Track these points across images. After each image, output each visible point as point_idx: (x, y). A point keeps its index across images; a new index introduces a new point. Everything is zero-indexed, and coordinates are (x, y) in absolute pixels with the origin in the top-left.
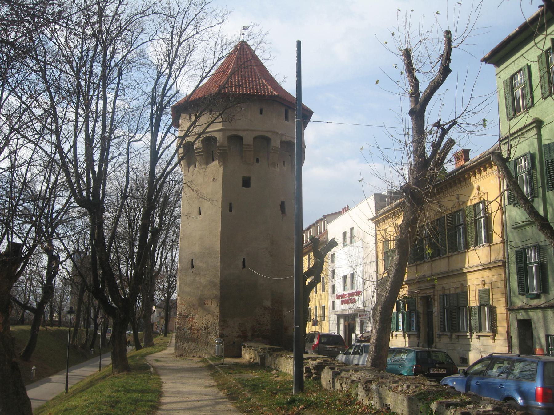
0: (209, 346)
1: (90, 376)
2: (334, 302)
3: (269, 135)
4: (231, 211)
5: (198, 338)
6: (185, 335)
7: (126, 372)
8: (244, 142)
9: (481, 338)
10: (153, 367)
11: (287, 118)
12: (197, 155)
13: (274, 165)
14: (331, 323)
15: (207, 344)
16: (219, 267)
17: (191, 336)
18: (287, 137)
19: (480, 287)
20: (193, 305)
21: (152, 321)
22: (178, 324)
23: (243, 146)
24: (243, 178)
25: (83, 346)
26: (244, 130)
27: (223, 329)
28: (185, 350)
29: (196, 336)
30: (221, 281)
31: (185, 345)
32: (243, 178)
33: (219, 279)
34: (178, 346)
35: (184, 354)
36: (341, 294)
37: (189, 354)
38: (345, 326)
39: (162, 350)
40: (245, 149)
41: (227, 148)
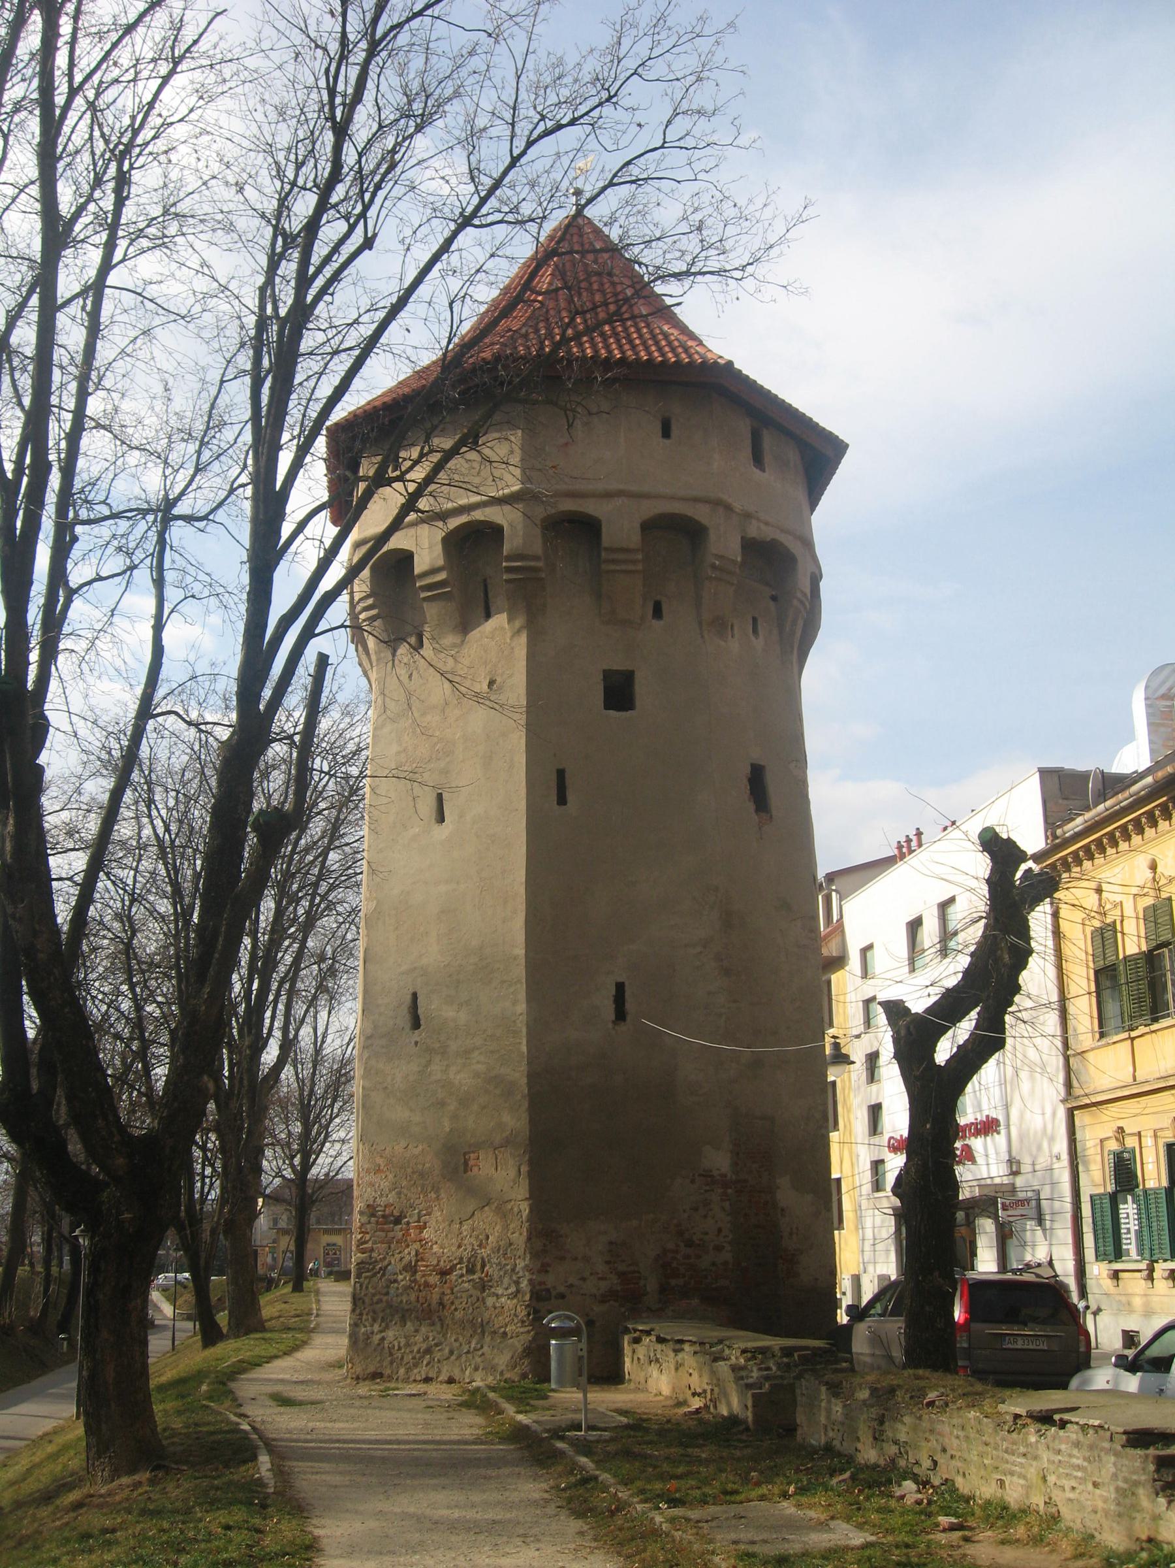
0: (488, 1339)
1: (47, 1437)
3: (701, 514)
4: (562, 800)
5: (441, 1304)
6: (392, 1291)
7: (144, 1476)
8: (606, 541)
9: (1121, 1275)
10: (271, 1447)
11: (758, 459)
13: (721, 626)
14: (869, 1234)
15: (480, 1328)
16: (524, 1018)
17: (413, 1297)
18: (763, 527)
19: (1113, 1146)
20: (422, 1175)
24: (607, 675)
25: (36, 1328)
26: (608, 495)
27: (544, 1269)
28: (391, 1354)
29: (435, 1298)
30: (532, 1077)
31: (390, 1334)
32: (607, 675)
33: (524, 1067)
34: (361, 1338)
35: (387, 1372)
37: (408, 1370)
40: (612, 567)
41: (540, 564)
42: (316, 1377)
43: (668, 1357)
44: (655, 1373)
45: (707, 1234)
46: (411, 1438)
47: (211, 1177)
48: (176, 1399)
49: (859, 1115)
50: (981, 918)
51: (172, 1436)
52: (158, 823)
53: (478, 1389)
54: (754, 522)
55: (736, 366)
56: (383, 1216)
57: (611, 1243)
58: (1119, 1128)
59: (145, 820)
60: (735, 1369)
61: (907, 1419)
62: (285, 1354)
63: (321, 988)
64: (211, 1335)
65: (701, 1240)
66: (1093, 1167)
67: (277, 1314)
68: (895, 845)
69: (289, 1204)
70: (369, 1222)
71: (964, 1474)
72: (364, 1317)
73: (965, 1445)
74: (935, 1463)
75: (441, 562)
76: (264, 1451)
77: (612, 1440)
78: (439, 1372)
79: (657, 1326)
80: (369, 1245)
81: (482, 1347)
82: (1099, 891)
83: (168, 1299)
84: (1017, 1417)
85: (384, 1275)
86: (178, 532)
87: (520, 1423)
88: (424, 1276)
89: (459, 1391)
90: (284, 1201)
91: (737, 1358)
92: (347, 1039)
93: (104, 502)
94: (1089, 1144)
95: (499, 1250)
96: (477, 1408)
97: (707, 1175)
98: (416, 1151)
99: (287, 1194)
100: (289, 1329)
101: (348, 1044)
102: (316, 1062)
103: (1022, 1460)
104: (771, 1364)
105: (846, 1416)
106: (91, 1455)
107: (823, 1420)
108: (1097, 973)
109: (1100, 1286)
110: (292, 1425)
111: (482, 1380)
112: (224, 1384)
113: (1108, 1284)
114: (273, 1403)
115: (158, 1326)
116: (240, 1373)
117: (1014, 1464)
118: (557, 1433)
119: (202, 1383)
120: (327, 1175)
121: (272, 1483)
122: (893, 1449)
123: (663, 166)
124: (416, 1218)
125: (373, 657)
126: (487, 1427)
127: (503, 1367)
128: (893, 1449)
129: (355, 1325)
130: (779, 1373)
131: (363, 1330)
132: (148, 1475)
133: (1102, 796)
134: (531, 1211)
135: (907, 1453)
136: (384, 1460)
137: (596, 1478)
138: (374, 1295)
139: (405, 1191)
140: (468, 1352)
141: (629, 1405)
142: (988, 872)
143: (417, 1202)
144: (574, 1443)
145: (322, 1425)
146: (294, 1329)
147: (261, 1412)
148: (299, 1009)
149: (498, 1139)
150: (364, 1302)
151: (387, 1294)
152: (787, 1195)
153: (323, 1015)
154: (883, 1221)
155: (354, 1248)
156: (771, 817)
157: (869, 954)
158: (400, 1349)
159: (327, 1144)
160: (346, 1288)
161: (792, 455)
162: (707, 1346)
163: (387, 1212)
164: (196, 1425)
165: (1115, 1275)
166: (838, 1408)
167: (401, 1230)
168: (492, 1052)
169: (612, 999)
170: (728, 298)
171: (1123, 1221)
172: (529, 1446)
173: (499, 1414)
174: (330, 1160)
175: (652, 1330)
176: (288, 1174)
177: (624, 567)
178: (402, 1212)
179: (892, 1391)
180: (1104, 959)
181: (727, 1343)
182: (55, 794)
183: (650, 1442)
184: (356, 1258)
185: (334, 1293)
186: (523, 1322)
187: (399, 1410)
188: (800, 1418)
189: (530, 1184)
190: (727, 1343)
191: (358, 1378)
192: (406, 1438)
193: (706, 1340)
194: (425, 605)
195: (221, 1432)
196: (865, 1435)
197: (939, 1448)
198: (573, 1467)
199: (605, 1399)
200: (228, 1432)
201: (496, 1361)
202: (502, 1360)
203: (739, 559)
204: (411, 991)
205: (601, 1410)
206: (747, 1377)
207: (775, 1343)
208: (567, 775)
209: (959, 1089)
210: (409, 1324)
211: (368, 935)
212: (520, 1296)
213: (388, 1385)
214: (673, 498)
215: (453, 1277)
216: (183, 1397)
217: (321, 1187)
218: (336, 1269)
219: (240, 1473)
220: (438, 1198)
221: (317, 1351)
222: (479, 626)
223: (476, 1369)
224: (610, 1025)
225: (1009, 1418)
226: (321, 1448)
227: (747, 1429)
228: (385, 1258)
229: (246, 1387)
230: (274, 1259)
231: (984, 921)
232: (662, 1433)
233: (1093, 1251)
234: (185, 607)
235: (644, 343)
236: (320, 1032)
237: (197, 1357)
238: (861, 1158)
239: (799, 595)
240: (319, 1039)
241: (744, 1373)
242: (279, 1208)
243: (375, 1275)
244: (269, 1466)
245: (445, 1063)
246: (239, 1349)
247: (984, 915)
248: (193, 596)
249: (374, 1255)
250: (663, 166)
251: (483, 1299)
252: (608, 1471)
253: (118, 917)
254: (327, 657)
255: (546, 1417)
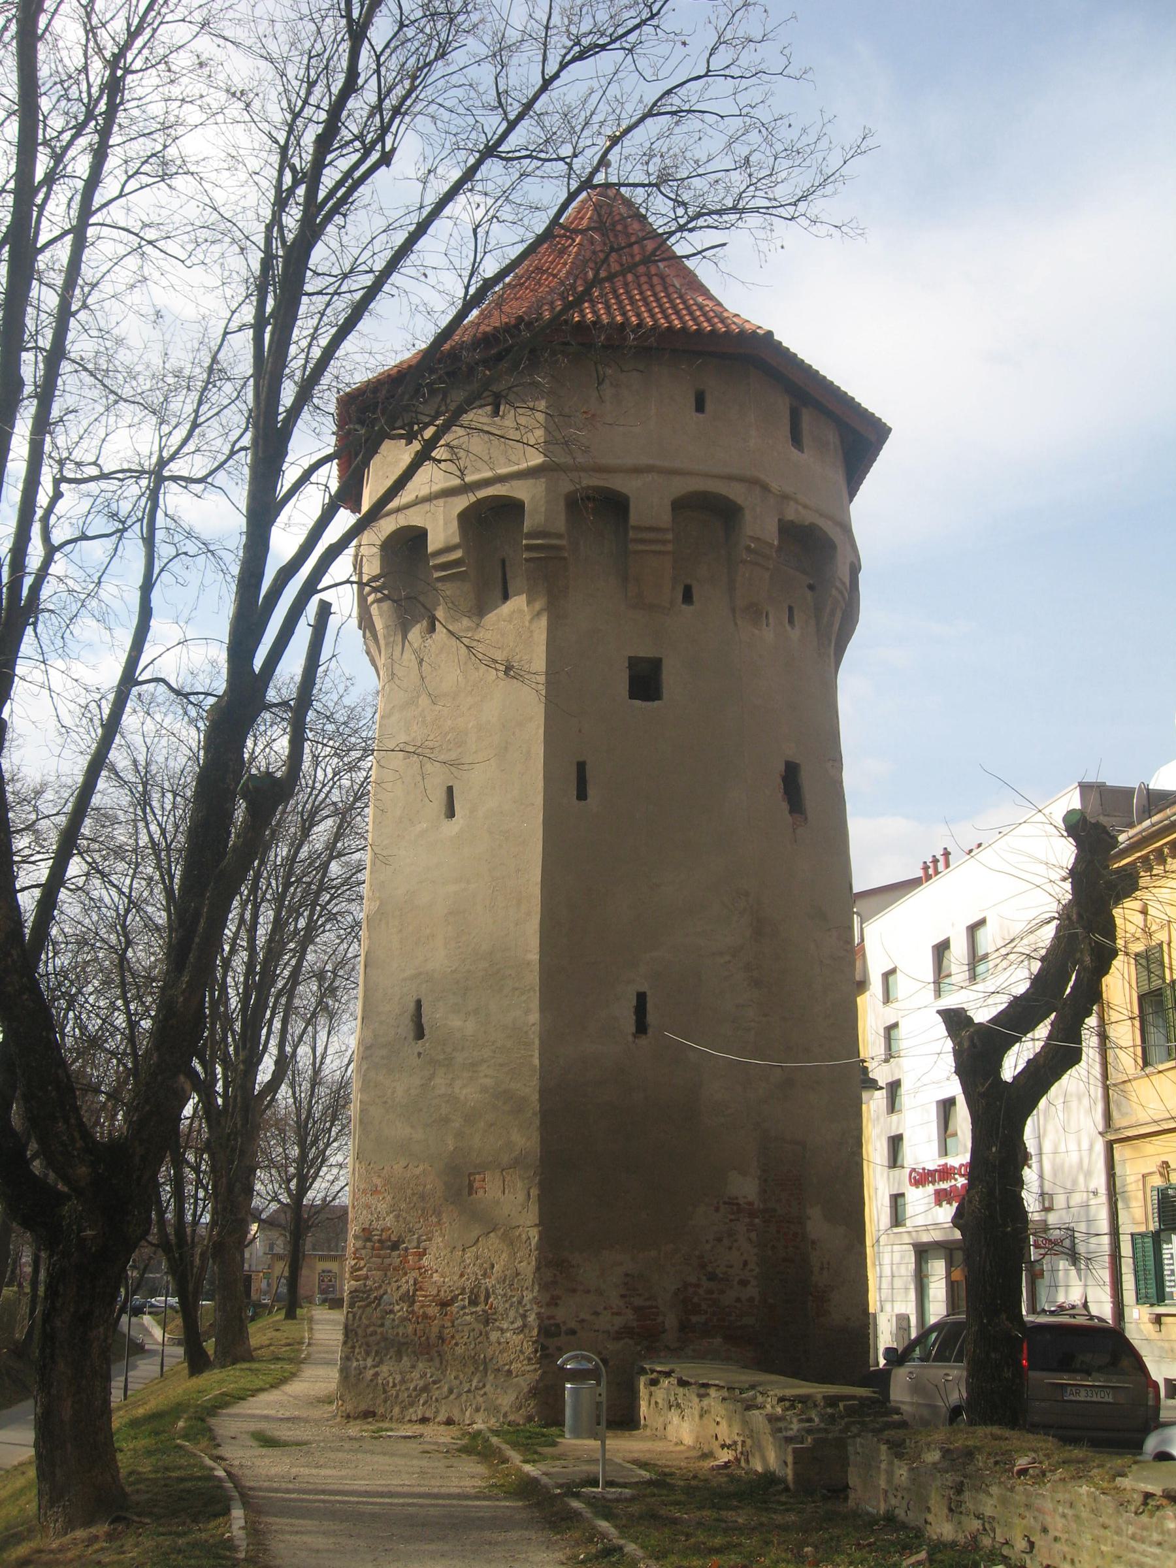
0: (491, 1377)
2: (897, 1200)
3: (735, 492)
4: (582, 795)
5: (441, 1338)
6: (388, 1323)
7: (102, 1529)
8: (633, 519)
9: (1164, 1319)
11: (796, 439)
12: (439, 579)
13: (755, 613)
15: (481, 1365)
16: (537, 1028)
17: (410, 1329)
18: (800, 508)
19: (1157, 1181)
20: (422, 1197)
21: (246, 1267)
22: (357, 1279)
23: (631, 534)
24: (633, 662)
26: (637, 470)
27: (554, 1302)
28: (385, 1392)
29: (435, 1330)
30: (544, 1093)
31: (384, 1369)
32: (633, 662)
33: (535, 1082)
35: (380, 1410)
36: (931, 1166)
38: (952, 1286)
39: (284, 1381)
40: (641, 547)
42: (303, 1413)
43: (693, 1404)
44: (676, 1420)
45: (731, 1267)
46: (406, 1489)
47: (204, 1200)
48: (150, 1435)
49: (878, 1145)
50: (1054, 918)
51: (138, 1482)
52: (154, 828)
53: (479, 1432)
54: (792, 503)
55: (776, 337)
56: (380, 1241)
57: (627, 1275)
58: (1164, 1162)
59: (141, 825)
60: (771, 1419)
61: (994, 1490)
62: (272, 1387)
63: (321, 1005)
64: (197, 1362)
65: (725, 1273)
66: (1133, 1204)
67: (267, 1342)
68: (921, 865)
69: (284, 1228)
70: (364, 1247)
71: (1072, 1561)
72: (357, 1350)
73: (1074, 1526)
74: (1032, 1544)
75: (456, 540)
76: (239, 1504)
77: (632, 1499)
78: (437, 1412)
79: (677, 1367)
80: (364, 1272)
81: (484, 1386)
82: (1144, 912)
83: (159, 1323)
84: (1148, 1496)
85: (379, 1305)
86: (174, 498)
87: (527, 1475)
88: (422, 1307)
89: (458, 1434)
90: (279, 1226)
91: (773, 1407)
92: (346, 1061)
93: (95, 463)
94: (1130, 1179)
95: (504, 1281)
96: (479, 1454)
97: (732, 1203)
98: (418, 1171)
99: (282, 1218)
100: (278, 1359)
101: (348, 1065)
102: (315, 1081)
103: (1157, 1550)
104: (813, 1414)
105: (913, 1480)
106: (44, 1502)
107: (883, 1484)
108: (1141, 998)
109: (1140, 1331)
110: (273, 1471)
111: (484, 1422)
112: (203, 1420)
113: (1149, 1328)
114: (255, 1444)
115: (149, 1351)
116: (219, 1407)
117: (1143, 1553)
118: (571, 1489)
119: (179, 1418)
120: (324, 1200)
121: (243, 1544)
122: (976, 1524)
123: (706, 96)
124: (414, 1244)
125: (382, 642)
126: (490, 1478)
127: (507, 1409)
128: (976, 1524)
129: (347, 1359)
130: (822, 1425)
131: (355, 1364)
132: (106, 1527)
133: (1147, 812)
134: (540, 1239)
135: (994, 1531)
136: (374, 1517)
137: (621, 1548)
138: (367, 1326)
139: (404, 1214)
140: (469, 1391)
141: (648, 1456)
142: (1072, 860)
143: (418, 1226)
144: (591, 1501)
145: (307, 1471)
146: (284, 1359)
147: (240, 1453)
148: (296, 1026)
149: (505, 1159)
150: (356, 1333)
151: (382, 1325)
152: (817, 1225)
153: (322, 1036)
154: (902, 1258)
155: (347, 1275)
156: (806, 819)
157: (891, 979)
158: (394, 1385)
159: (324, 1169)
160: (339, 1316)
161: (832, 437)
162: (737, 1392)
163: (384, 1237)
164: (167, 1469)
165: (1158, 1320)
166: (902, 1473)
167: (399, 1256)
168: (501, 1065)
169: (633, 1010)
170: (772, 248)
171: (1166, 1262)
172: (538, 1504)
173: (503, 1463)
174: (328, 1184)
175: (672, 1371)
176: (285, 1199)
177: (653, 547)
178: (400, 1237)
179: (969, 1454)
180: (1150, 982)
181: (761, 1389)
182: (51, 798)
183: (677, 1503)
184: (348, 1286)
185: (328, 1322)
186: (530, 1359)
187: (393, 1455)
188: (853, 1480)
189: (540, 1209)
190: (761, 1389)
191: (348, 1416)
192: (400, 1489)
193: (736, 1385)
194: (439, 585)
195: (192, 1478)
196: (937, 1504)
197: (1039, 1528)
198: (593, 1535)
199: (623, 1446)
200: (199, 1478)
201: (499, 1401)
202: (506, 1401)
203: (776, 543)
204: (415, 998)
205: (619, 1461)
206: (786, 1429)
207: (818, 1391)
208: (588, 767)
209: (1030, 1105)
210: (405, 1359)
211: (370, 938)
212: (526, 1331)
213: (381, 1425)
214: (707, 476)
215: (454, 1308)
216: (157, 1434)
217: (318, 1212)
218: (331, 1296)
219: (207, 1531)
220: (439, 1223)
221: (306, 1385)
222: (496, 607)
223: (477, 1410)
224: (630, 1038)
225: (1138, 1498)
226: (302, 1500)
227: (787, 1489)
228: (380, 1287)
229: (227, 1425)
230: (269, 1285)
231: (1056, 922)
232: (689, 1491)
233: (1133, 1294)
234: (175, 566)
235: (677, 313)
236: (319, 1050)
237: (183, 1387)
238: (880, 1192)
239: (838, 584)
240: (318, 1060)
241: (781, 1425)
242: (274, 1234)
243: (369, 1305)
244: (242, 1523)
245: (451, 1076)
246: (224, 1381)
247: (1056, 915)
248: (186, 553)
249: (369, 1283)
250: (706, 96)
251: (487, 1334)
252: (635, 1540)
253: (113, 927)
254: (330, 605)
255: (555, 1468)
